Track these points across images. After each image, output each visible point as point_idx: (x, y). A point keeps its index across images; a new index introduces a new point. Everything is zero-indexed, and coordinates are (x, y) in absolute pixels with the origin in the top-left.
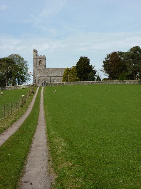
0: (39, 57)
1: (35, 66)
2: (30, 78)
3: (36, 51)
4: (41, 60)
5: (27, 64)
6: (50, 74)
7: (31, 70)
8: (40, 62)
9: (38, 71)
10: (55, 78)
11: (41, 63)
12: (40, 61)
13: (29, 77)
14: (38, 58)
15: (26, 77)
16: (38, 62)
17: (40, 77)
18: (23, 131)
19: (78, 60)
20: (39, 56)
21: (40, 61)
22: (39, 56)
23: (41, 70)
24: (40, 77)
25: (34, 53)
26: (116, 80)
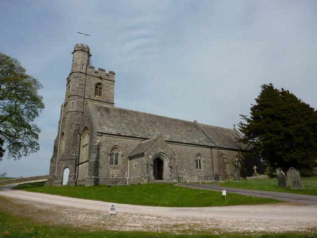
0: (96, 72)
2: (38, 142)
4: (99, 84)
6: (148, 129)
8: (96, 87)
9: (102, 115)
13: (35, 140)
14: (93, 74)
16: (90, 89)
17: (119, 135)
22: (96, 69)
24: (119, 135)
25: (81, 53)
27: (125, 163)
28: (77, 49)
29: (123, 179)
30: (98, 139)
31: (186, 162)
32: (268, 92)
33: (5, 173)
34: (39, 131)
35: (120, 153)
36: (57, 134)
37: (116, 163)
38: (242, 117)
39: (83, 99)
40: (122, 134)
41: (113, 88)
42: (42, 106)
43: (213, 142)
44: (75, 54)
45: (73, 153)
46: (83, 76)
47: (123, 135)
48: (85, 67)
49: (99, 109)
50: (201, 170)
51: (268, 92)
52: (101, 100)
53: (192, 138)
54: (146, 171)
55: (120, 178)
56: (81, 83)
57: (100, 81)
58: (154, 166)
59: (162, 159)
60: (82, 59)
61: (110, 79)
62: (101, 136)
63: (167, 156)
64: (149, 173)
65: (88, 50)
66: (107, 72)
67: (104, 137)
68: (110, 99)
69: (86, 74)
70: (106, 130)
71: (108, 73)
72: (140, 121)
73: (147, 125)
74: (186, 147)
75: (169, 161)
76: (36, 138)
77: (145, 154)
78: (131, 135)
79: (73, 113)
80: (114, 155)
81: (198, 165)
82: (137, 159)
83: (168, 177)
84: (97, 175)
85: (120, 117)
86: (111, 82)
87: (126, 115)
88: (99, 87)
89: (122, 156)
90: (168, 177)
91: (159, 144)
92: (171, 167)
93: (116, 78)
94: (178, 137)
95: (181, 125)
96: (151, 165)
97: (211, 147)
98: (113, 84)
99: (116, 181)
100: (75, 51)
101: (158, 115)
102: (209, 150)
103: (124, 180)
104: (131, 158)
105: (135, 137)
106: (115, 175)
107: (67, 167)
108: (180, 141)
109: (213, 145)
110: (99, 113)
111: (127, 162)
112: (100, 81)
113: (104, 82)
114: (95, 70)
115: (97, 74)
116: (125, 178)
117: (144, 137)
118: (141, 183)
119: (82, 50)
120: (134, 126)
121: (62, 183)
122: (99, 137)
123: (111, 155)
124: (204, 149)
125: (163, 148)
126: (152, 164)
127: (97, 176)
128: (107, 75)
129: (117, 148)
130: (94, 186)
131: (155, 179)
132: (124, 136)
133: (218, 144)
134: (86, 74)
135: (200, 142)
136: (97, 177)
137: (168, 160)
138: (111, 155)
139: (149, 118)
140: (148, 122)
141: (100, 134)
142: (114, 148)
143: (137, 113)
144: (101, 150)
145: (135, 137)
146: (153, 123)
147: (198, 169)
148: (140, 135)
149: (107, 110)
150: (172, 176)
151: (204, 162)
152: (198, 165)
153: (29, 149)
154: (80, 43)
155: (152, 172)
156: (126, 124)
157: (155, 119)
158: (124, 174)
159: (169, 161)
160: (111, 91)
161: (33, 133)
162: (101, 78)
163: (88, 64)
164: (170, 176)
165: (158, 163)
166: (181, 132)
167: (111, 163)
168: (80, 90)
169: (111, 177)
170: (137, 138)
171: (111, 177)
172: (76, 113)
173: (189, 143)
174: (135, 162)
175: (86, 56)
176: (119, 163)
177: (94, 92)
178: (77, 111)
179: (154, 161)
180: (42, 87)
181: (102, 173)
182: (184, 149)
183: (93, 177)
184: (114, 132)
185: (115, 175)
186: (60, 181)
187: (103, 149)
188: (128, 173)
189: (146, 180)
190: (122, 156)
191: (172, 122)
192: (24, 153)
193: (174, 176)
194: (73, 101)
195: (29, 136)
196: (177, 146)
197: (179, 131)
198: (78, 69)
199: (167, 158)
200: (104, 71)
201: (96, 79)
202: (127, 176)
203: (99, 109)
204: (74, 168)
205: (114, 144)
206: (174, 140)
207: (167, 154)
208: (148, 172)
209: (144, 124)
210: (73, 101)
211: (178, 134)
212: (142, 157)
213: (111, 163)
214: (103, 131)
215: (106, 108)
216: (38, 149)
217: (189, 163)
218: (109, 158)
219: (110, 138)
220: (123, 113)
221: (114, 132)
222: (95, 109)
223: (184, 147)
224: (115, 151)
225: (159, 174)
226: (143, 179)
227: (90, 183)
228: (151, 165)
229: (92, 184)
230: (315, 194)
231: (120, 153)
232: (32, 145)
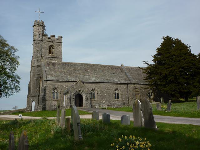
0: (49, 38)
1: (37, 56)
2: (19, 85)
3: (41, 25)
4: (52, 46)
5: (17, 54)
6: (80, 75)
7: (24, 70)
8: (50, 48)
9: (50, 68)
10: (94, 86)
11: (52, 53)
12: (51, 48)
13: (17, 84)
14: (47, 40)
15: (10, 83)
16: (46, 50)
17: (58, 81)
18: (27, 110)
19: (159, 43)
20: (49, 36)
21: (51, 48)
22: (49, 36)
23: (57, 66)
24: (58, 81)
25: (38, 27)
26: (184, 92)
27: (62, 97)
28: (35, 24)
30: (45, 84)
32: (168, 41)
33: (16, 107)
34: (20, 78)
35: (59, 91)
36: (29, 81)
37: (57, 97)
38: (145, 63)
39: (41, 57)
41: (61, 47)
42: (18, 63)
43: (130, 81)
44: (35, 27)
45: (36, 92)
46: (40, 42)
47: (61, 80)
48: (41, 36)
49: (48, 64)
50: (119, 100)
51: (168, 41)
52: (53, 56)
54: (69, 102)
56: (39, 47)
57: (52, 44)
58: (76, 99)
60: (39, 31)
61: (59, 41)
62: (46, 82)
64: (72, 103)
65: (43, 23)
66: (57, 37)
67: (48, 83)
68: (59, 55)
69: (42, 41)
70: (50, 78)
71: (57, 37)
72: (75, 70)
74: (123, 85)
76: (18, 83)
77: (69, 92)
79: (35, 67)
81: (116, 96)
84: (45, 105)
86: (59, 44)
87: (67, 66)
88: (51, 48)
89: (61, 93)
91: (79, 86)
93: (63, 40)
94: (102, 79)
96: (73, 98)
97: (128, 84)
98: (61, 45)
100: (34, 26)
102: (125, 86)
104: (65, 94)
105: (69, 81)
107: (33, 101)
108: (102, 81)
109: (129, 82)
110: (47, 67)
111: (64, 97)
112: (52, 44)
113: (55, 44)
114: (48, 37)
115: (50, 39)
117: (75, 81)
119: (38, 25)
120: (70, 74)
121: (31, 110)
122: (45, 83)
123: (53, 93)
124: (122, 86)
127: (45, 105)
128: (57, 39)
130: (42, 111)
132: (61, 81)
133: (134, 81)
134: (42, 41)
135: (119, 81)
136: (44, 106)
138: (53, 93)
139: (84, 66)
140: (81, 70)
141: (46, 81)
142: (55, 89)
143: (75, 64)
144: (47, 91)
145: (69, 81)
146: (86, 70)
147: (116, 100)
149: (54, 64)
151: (121, 94)
152: (116, 96)
153: (15, 90)
154: (37, 20)
155: (73, 102)
156: (64, 72)
157: (88, 67)
159: (85, 96)
161: (16, 79)
162: (52, 42)
163: (43, 33)
164: (87, 104)
167: (116, 98)
168: (39, 52)
169: (54, 106)
170: (70, 81)
171: (54, 106)
172: (37, 67)
173: (109, 82)
175: (42, 28)
176: (59, 98)
177: (48, 52)
178: (37, 66)
180: (18, 51)
181: (48, 104)
183: (41, 106)
184: (55, 79)
186: (30, 109)
187: (48, 90)
190: (61, 93)
191: (102, 68)
192: (12, 93)
194: (35, 60)
195: (14, 82)
196: (100, 85)
198: (37, 38)
200: (54, 36)
201: (49, 42)
203: (48, 64)
204: (37, 102)
205: (54, 86)
206: (97, 81)
210: (35, 60)
213: (116, 98)
214: (48, 79)
216: (20, 90)
217: (109, 95)
218: (52, 95)
219: (52, 83)
220: (65, 65)
221: (55, 79)
222: (46, 65)
227: (40, 110)
228: (73, 98)
229: (41, 110)
230: (198, 117)
231: (59, 91)
232: (16, 88)
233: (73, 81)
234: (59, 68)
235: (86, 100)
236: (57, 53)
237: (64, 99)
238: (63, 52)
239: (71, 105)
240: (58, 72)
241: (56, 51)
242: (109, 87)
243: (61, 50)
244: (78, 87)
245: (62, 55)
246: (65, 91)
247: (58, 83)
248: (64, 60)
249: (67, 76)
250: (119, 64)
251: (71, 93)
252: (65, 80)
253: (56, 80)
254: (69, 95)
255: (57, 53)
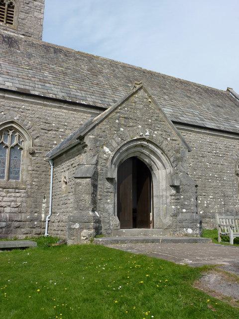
27: (40, 174)
29: (32, 220)
31: (213, 178)
35: (27, 145)
40: (33, 92)
47: (37, 93)
53: (227, 120)
54: (88, 198)
55: (22, 217)
58: (120, 184)
59: (147, 160)
63: (163, 152)
64: (100, 205)
73: (115, 82)
75: (170, 169)
77: (87, 140)
78: (60, 96)
80: (8, 151)
82: (68, 163)
83: (168, 220)
85: (42, 57)
89: (33, 154)
90: (168, 220)
92: (176, 188)
95: (198, 93)
96: (110, 180)
99: (8, 226)
101: (144, 68)
103: (35, 222)
104: (56, 160)
106: (8, 209)
108: (200, 123)
116: (38, 219)
117: (99, 105)
118: (70, 243)
120: (76, 80)
125: (150, 126)
126: (115, 175)
129: (17, 131)
131: (123, 225)
137: (168, 165)
148: (90, 101)
150: (180, 217)
155: (109, 204)
156: (53, 72)
157: (136, 74)
158: (37, 205)
159: (170, 169)
160: (36, 14)
164: (175, 215)
165: (135, 176)
166: (200, 105)
173: (222, 128)
174: (65, 172)
176: (24, 176)
179: (122, 167)
182: (210, 143)
185: (8, 209)
188: (47, 203)
189: (85, 232)
190: (33, 154)
193: (188, 216)
197: (193, 103)
199: (163, 157)
202: (47, 212)
207: (163, 146)
208: (94, 202)
209: (108, 79)
211: (192, 107)
212: (79, 153)
215: (9, 38)
217: (221, 179)
223: (209, 139)
224: (9, 138)
225: (136, 207)
226: (77, 226)
228: (110, 180)
233: (91, 104)
234: (30, 56)
235: (174, 192)
236: (24, 22)
237: (47, 183)
238: (45, 23)
239: (98, 221)
240: (28, 65)
241: (22, 15)
242: (219, 145)
243: (41, 16)
244: (136, 120)
245: (41, 31)
246: (57, 145)
247: (25, 105)
248: (49, 37)
249: (64, 85)
250: (223, 88)
251: (97, 150)
252: (60, 97)
253: (14, 89)
254: (85, 160)
255: (24, 22)
